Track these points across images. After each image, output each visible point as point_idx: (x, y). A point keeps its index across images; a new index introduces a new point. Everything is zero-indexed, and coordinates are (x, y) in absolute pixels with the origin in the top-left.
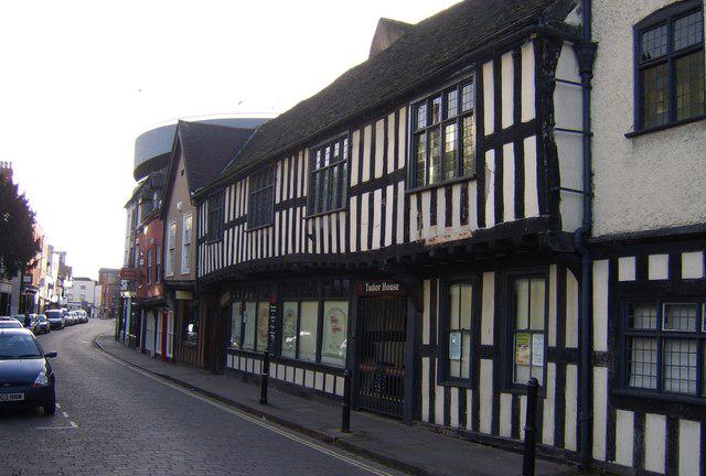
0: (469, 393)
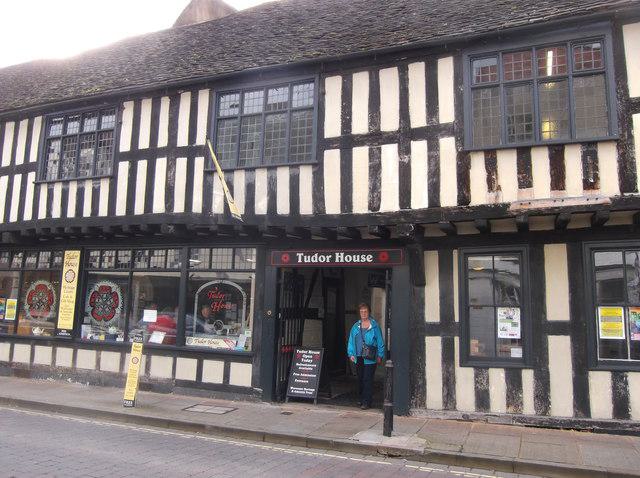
0: (528, 377)
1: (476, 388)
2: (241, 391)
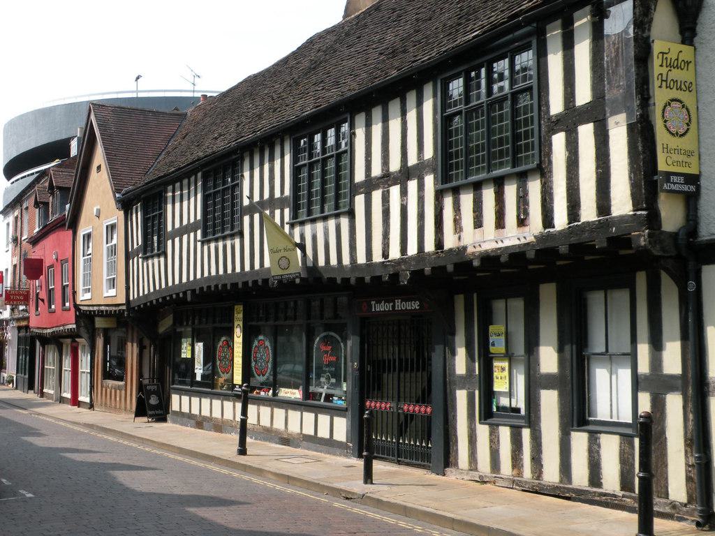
0: (526, 433)
1: (491, 447)
2: (339, 445)
